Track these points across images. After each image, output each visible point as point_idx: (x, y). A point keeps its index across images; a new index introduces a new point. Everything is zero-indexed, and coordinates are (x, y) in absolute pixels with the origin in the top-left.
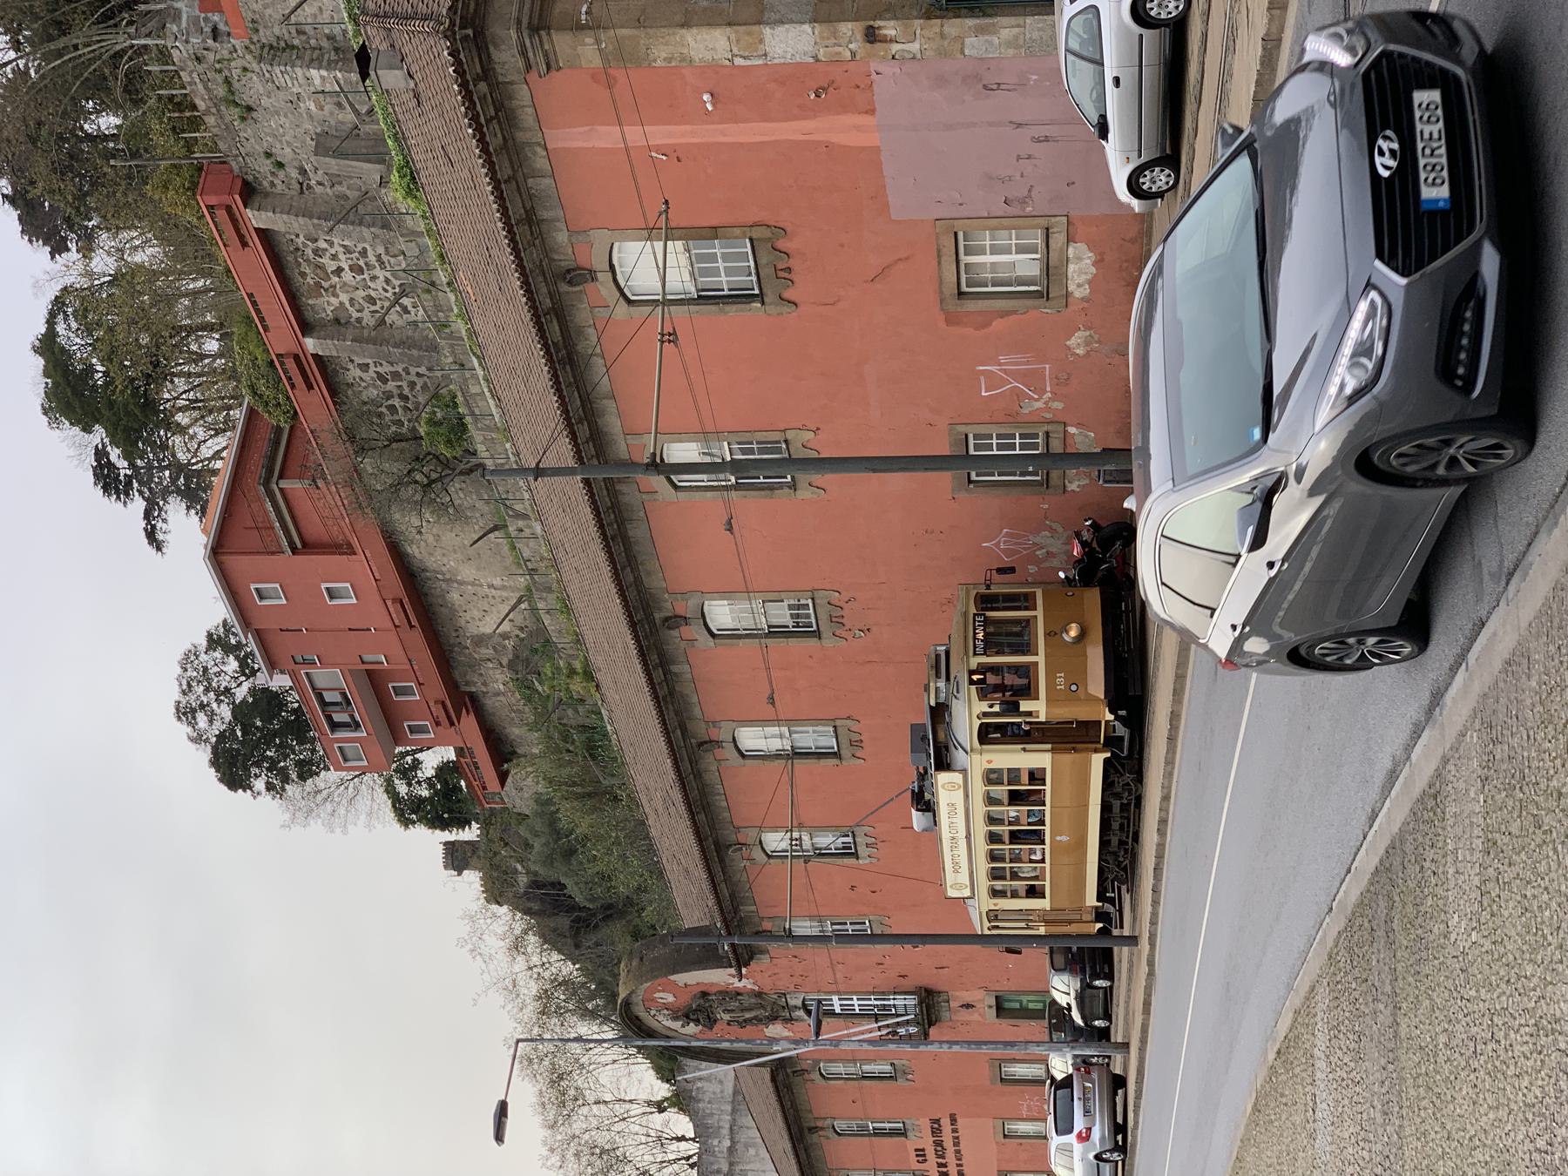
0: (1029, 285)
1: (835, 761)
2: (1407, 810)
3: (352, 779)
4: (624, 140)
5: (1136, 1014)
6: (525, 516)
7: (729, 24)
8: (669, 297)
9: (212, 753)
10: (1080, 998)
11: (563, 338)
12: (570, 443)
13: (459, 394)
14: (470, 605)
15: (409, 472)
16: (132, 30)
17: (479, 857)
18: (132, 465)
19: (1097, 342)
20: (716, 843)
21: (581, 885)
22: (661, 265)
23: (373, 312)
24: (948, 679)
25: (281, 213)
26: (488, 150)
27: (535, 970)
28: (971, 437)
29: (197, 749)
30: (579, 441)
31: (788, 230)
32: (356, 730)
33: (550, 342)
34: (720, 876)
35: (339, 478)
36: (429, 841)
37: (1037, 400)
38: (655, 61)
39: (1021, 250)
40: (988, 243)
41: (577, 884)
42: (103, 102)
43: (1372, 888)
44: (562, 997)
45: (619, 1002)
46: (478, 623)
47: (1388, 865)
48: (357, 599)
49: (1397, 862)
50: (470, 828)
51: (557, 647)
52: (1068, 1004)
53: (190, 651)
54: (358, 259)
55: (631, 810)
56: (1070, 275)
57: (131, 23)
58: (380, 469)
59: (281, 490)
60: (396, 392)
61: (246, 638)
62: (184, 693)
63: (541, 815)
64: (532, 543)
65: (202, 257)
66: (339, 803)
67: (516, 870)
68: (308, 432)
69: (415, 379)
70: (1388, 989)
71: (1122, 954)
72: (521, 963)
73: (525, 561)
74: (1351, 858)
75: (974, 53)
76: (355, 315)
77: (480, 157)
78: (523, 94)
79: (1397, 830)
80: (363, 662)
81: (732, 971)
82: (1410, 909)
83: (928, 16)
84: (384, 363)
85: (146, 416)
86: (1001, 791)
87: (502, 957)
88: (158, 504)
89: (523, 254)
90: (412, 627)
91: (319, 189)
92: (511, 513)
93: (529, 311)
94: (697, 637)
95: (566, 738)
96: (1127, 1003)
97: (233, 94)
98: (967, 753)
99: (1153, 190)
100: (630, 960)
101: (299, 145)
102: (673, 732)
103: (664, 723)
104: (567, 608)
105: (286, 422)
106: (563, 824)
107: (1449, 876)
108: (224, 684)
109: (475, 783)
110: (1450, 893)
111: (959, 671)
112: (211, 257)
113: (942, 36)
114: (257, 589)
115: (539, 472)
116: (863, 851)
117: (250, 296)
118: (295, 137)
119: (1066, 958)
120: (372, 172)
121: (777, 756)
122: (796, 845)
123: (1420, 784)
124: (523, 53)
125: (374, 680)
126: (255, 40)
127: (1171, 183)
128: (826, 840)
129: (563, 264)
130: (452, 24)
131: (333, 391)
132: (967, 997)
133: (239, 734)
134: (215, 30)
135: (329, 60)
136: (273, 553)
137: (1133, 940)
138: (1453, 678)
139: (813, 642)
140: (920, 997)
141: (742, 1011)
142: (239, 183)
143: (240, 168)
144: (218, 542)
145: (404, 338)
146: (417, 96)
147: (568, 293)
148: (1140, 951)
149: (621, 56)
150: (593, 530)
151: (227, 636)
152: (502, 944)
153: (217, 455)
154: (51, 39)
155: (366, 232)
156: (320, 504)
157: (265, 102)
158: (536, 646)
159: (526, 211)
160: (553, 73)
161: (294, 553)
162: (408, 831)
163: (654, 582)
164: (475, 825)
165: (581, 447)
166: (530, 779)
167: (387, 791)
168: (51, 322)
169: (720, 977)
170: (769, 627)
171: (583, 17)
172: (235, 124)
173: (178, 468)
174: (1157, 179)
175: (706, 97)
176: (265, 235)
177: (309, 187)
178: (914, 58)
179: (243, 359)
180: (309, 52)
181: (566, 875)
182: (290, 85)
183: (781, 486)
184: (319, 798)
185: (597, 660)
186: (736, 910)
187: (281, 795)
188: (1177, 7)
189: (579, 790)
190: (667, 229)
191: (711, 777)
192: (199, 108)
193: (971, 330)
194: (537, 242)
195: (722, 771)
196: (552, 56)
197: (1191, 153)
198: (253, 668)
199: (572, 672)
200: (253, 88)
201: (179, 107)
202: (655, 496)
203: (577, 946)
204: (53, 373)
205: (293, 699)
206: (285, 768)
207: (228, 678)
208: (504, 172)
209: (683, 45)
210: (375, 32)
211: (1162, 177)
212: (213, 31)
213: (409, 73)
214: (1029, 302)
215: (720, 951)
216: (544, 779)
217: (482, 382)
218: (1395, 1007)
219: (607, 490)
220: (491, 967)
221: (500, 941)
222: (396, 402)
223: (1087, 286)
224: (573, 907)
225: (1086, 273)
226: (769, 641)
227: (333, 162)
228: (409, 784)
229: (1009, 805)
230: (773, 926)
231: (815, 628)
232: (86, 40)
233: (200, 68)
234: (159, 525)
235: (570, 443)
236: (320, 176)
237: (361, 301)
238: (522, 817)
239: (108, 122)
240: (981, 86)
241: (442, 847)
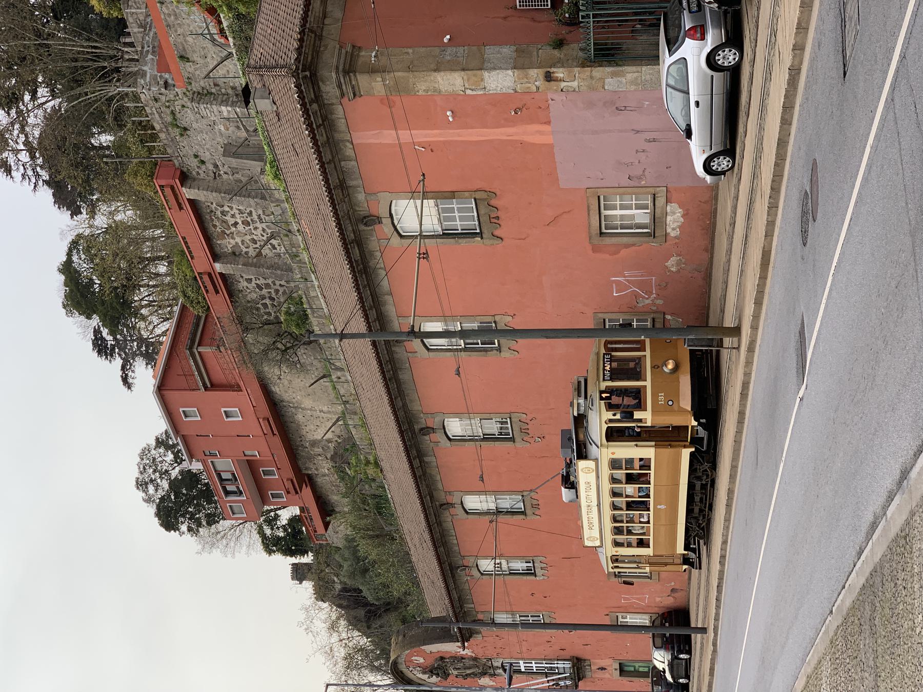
0: (643, 228)
1: (523, 517)
2: (885, 547)
3: (238, 525)
4: (398, 138)
5: (705, 676)
6: (342, 369)
7: (463, 70)
8: (424, 234)
9: (157, 509)
10: (671, 665)
11: (362, 258)
12: (364, 321)
13: (304, 296)
14: (309, 423)
15: (274, 343)
16: (118, 84)
17: (312, 573)
18: (115, 339)
19: (683, 264)
20: (450, 565)
21: (371, 591)
22: (420, 214)
23: (254, 248)
24: (586, 397)
25: (203, 190)
26: (317, 144)
27: (344, 641)
28: (607, 320)
29: (148, 506)
30: (370, 320)
31: (498, 194)
32: (240, 496)
33: (353, 260)
34: (452, 586)
35: (233, 346)
36: (283, 563)
37: (647, 299)
38: (418, 91)
39: (638, 207)
40: (618, 203)
41: (369, 589)
42: (102, 127)
43: (861, 598)
44: (360, 658)
45: (391, 662)
46: (313, 433)
47: (871, 583)
48: (242, 418)
49: (878, 580)
50: (308, 556)
51: (359, 448)
52: (663, 669)
53: (145, 448)
54: (247, 217)
55: (401, 545)
56: (668, 222)
57: (118, 80)
58: (257, 341)
59: (199, 353)
60: (267, 295)
61: (177, 440)
62: (141, 473)
63: (349, 548)
64: (345, 385)
65: (158, 217)
66: (230, 540)
67: (334, 581)
68: (216, 318)
69: (279, 288)
70: (871, 663)
71: (697, 638)
72: (335, 638)
73: (341, 396)
74: (845, 579)
75: (611, 88)
76: (244, 250)
77: (313, 148)
78: (339, 111)
79: (878, 560)
80: (245, 455)
81: (459, 644)
82: (887, 611)
83: (583, 66)
84: (261, 278)
85: (123, 310)
86: (621, 474)
87: (324, 634)
88: (129, 362)
89: (337, 207)
90: (274, 434)
91: (225, 177)
92: (333, 367)
93: (341, 241)
94: (440, 440)
95: (364, 502)
96: (700, 668)
97: (176, 120)
98: (598, 447)
99: (719, 170)
100: (398, 636)
101: (214, 151)
102: (425, 497)
103: (419, 492)
104: (364, 425)
105: (203, 312)
106: (361, 553)
107: (916, 590)
108: (165, 468)
109: (310, 529)
110: (916, 601)
111: (593, 392)
112: (163, 217)
113: (592, 77)
114: (184, 411)
115: (342, 336)
116: (539, 572)
117: (184, 238)
118: (212, 146)
119: (663, 639)
120: (256, 166)
121: (488, 513)
122: (498, 567)
123: (894, 530)
124: (340, 86)
125: (252, 466)
126: (189, 89)
127: (730, 166)
128: (520, 565)
129: (361, 213)
130: (297, 68)
131: (231, 295)
132: (602, 663)
133: (173, 497)
134: (166, 83)
135: (232, 101)
136: (194, 390)
137: (703, 630)
138: (916, 461)
139: (510, 444)
140: (573, 663)
141: (465, 669)
142: (178, 173)
143: (180, 163)
144: (161, 384)
145: (273, 263)
146: (278, 115)
147: (364, 230)
148: (708, 637)
149: (398, 89)
150: (378, 375)
151: (167, 440)
152: (324, 625)
153: (164, 333)
154: (72, 89)
155: (252, 201)
156: (221, 361)
157: (195, 125)
158: (348, 447)
159: (340, 181)
160: (357, 99)
161: (205, 390)
162: (271, 557)
163: (415, 407)
164: (310, 554)
165: (371, 324)
166: (342, 527)
167: (259, 533)
168: (69, 254)
169: (451, 648)
170: (484, 435)
171: (373, 59)
172: (177, 138)
173: (141, 340)
174: (721, 163)
175: (449, 113)
176: (192, 203)
177: (219, 175)
178: (574, 91)
179: (178, 275)
180: (221, 96)
181: (362, 584)
182: (209, 115)
183: (492, 349)
184: (219, 536)
185: (382, 454)
186: (462, 607)
187: (196, 534)
188: (734, 59)
189: (371, 533)
190: (424, 193)
191: (448, 525)
192: (156, 128)
193: (608, 255)
194: (346, 200)
195: (453, 520)
196: (356, 88)
197: (743, 147)
198: (182, 458)
199: (368, 463)
200: (188, 117)
201: (145, 128)
202: (415, 355)
203: (369, 627)
204: (70, 284)
205: (204, 478)
206: (199, 518)
207: (167, 464)
208: (327, 157)
209: (435, 82)
210: (254, 78)
211: (725, 162)
212: (165, 83)
213: (273, 101)
214: (642, 239)
215: (452, 632)
216: (351, 526)
217: (317, 289)
218: (876, 675)
219: (387, 349)
220: (318, 639)
221: (323, 624)
222: (268, 301)
223: (678, 230)
224: (367, 604)
225: (678, 222)
226: (482, 443)
227: (234, 160)
228: (272, 529)
229: (626, 483)
230: (484, 617)
231: (511, 436)
232: (92, 89)
233: (157, 105)
234: (130, 374)
235: (364, 321)
236: (226, 169)
237: (248, 242)
238: (338, 549)
239: (106, 139)
240: (615, 108)
241: (291, 566)
